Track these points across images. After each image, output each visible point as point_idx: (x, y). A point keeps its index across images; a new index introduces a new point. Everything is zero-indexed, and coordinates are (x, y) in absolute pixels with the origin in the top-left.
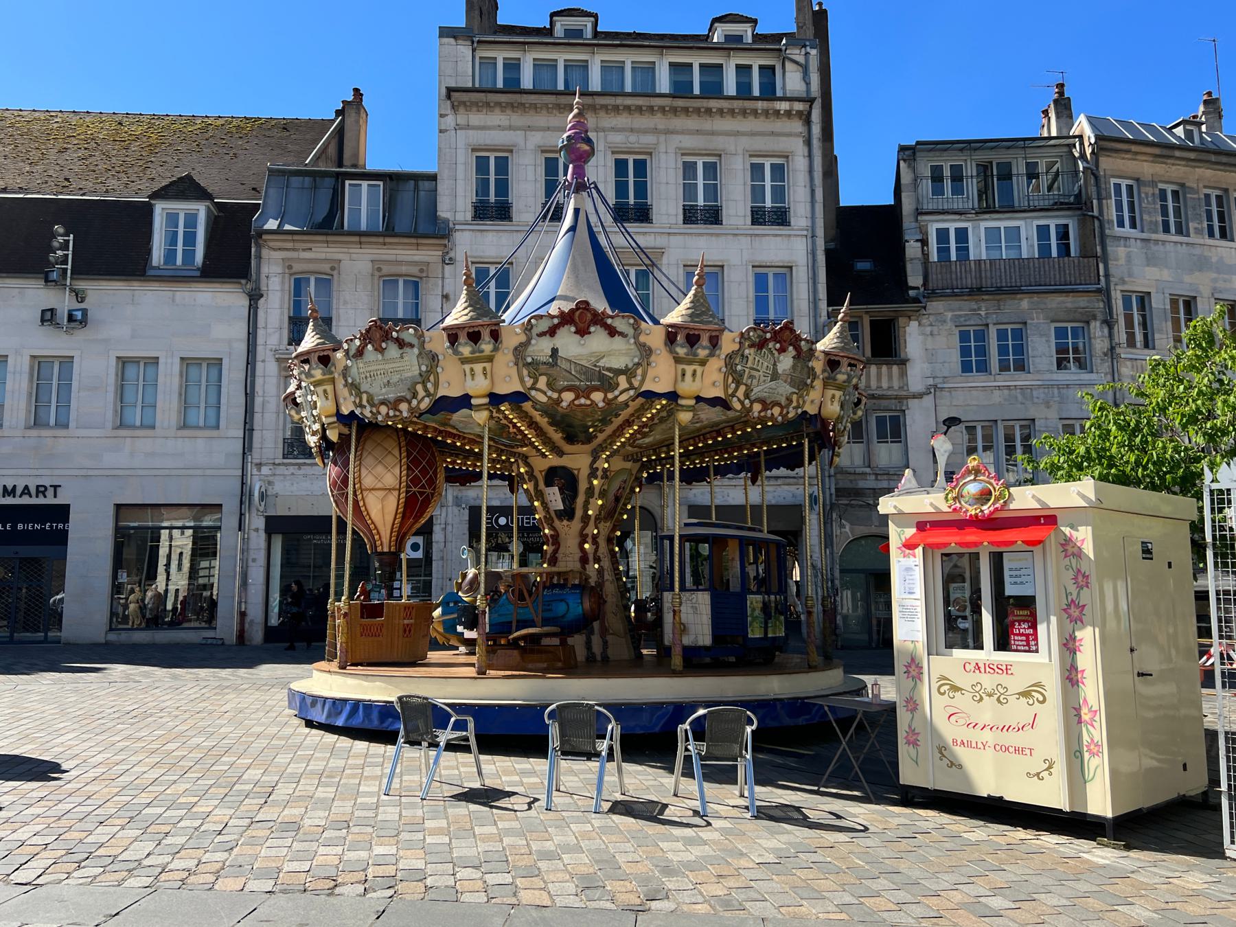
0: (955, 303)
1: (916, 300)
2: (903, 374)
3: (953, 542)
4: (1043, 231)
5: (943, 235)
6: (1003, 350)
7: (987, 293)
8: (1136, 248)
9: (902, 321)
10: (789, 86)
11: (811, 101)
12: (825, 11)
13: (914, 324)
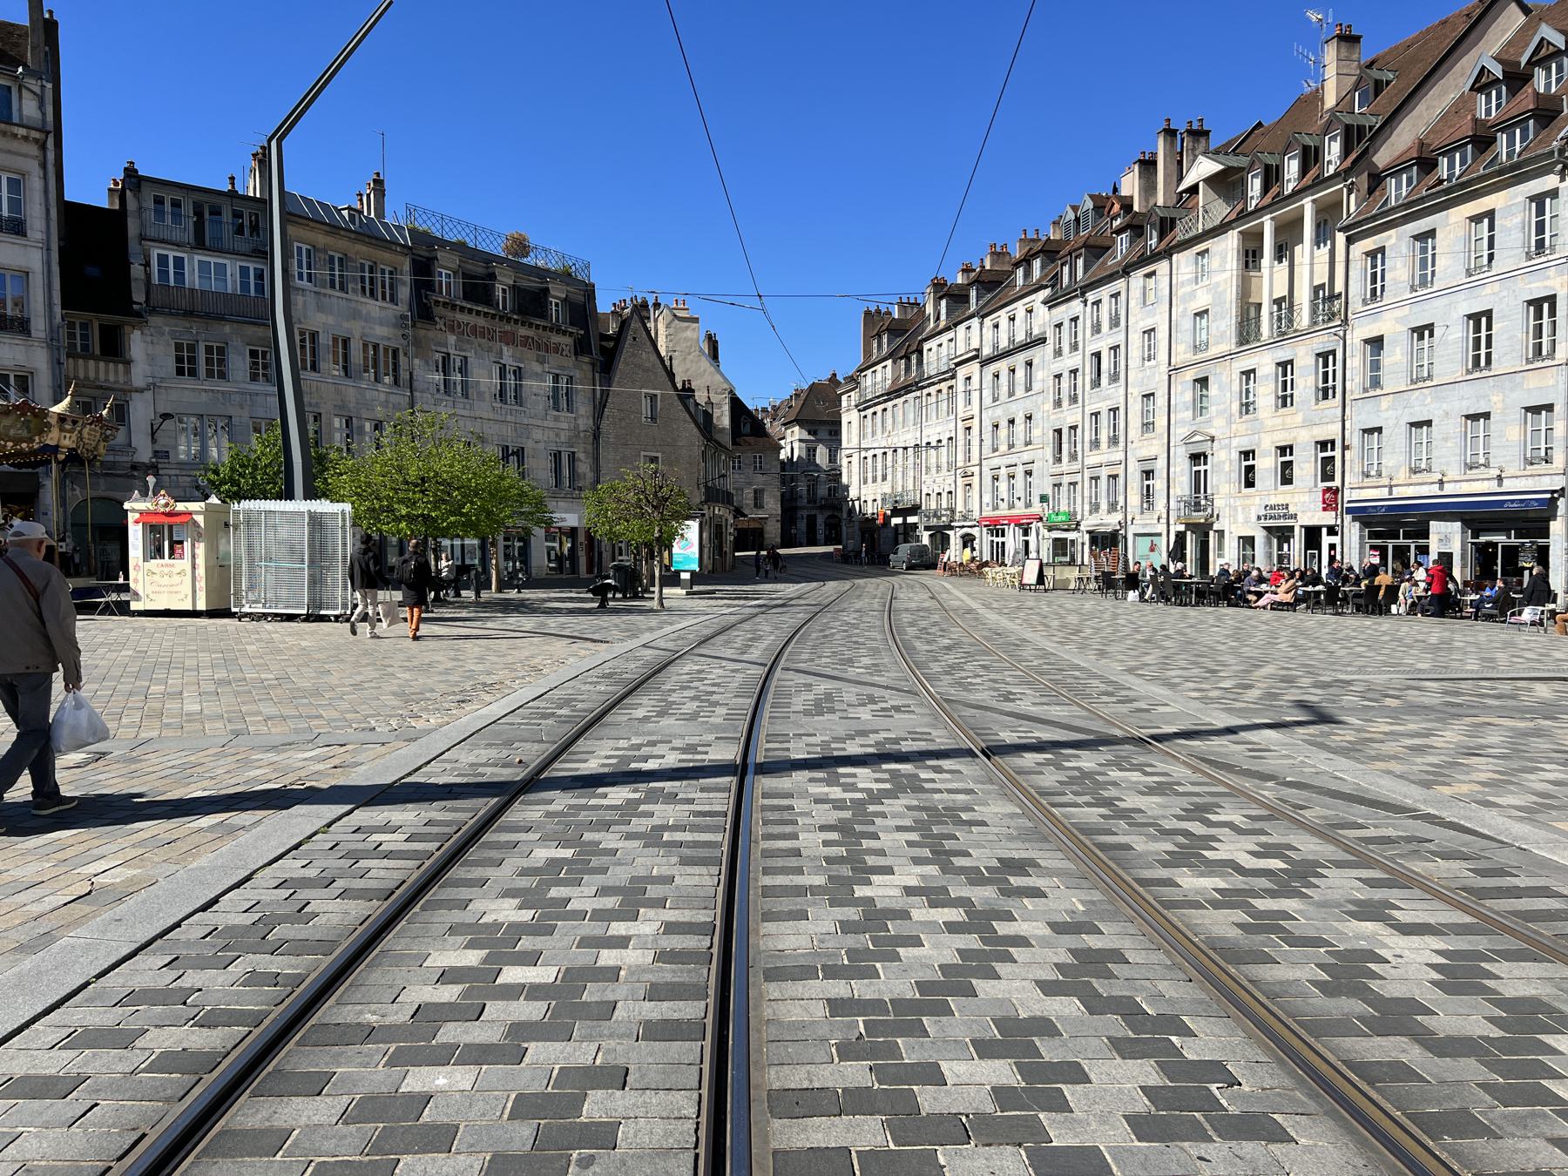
0: (173, 321)
1: (138, 315)
2: (128, 372)
3: (154, 520)
4: (244, 271)
5: (163, 260)
6: (209, 361)
7: (198, 316)
8: (310, 298)
9: (127, 329)
10: (26, 112)
11: (48, 133)
12: (56, 23)
13: (137, 333)
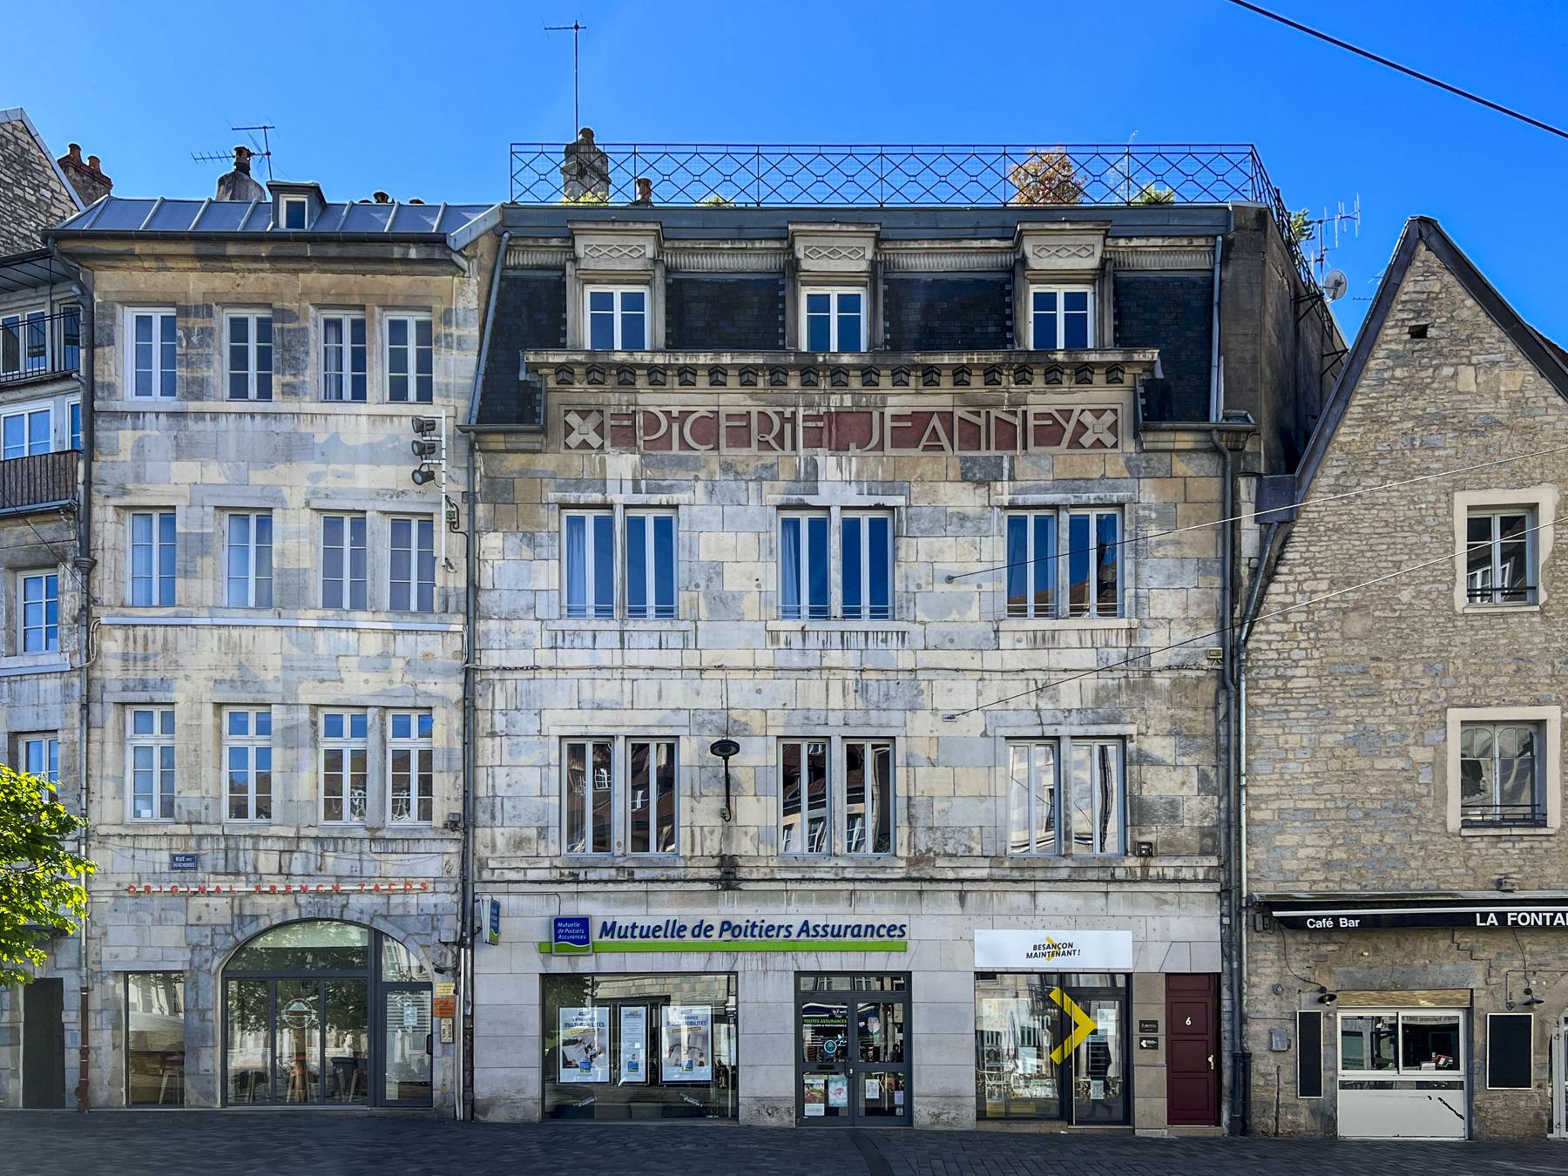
8: (156, 432)
